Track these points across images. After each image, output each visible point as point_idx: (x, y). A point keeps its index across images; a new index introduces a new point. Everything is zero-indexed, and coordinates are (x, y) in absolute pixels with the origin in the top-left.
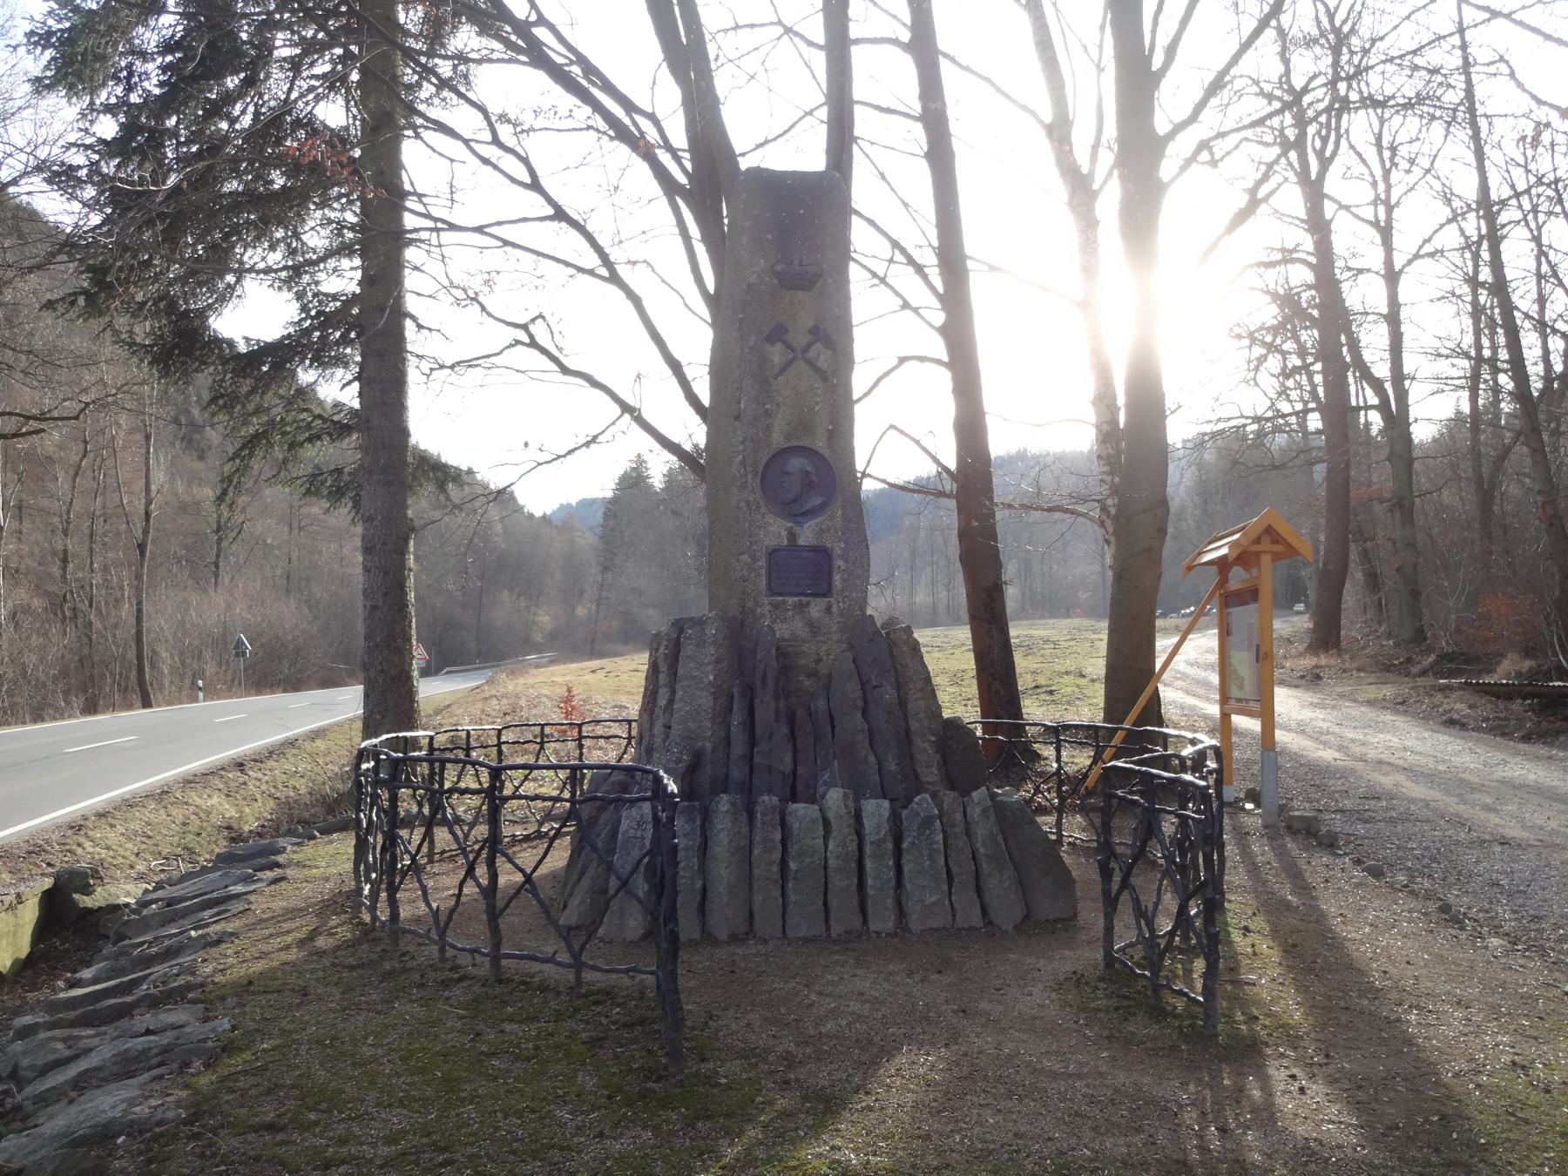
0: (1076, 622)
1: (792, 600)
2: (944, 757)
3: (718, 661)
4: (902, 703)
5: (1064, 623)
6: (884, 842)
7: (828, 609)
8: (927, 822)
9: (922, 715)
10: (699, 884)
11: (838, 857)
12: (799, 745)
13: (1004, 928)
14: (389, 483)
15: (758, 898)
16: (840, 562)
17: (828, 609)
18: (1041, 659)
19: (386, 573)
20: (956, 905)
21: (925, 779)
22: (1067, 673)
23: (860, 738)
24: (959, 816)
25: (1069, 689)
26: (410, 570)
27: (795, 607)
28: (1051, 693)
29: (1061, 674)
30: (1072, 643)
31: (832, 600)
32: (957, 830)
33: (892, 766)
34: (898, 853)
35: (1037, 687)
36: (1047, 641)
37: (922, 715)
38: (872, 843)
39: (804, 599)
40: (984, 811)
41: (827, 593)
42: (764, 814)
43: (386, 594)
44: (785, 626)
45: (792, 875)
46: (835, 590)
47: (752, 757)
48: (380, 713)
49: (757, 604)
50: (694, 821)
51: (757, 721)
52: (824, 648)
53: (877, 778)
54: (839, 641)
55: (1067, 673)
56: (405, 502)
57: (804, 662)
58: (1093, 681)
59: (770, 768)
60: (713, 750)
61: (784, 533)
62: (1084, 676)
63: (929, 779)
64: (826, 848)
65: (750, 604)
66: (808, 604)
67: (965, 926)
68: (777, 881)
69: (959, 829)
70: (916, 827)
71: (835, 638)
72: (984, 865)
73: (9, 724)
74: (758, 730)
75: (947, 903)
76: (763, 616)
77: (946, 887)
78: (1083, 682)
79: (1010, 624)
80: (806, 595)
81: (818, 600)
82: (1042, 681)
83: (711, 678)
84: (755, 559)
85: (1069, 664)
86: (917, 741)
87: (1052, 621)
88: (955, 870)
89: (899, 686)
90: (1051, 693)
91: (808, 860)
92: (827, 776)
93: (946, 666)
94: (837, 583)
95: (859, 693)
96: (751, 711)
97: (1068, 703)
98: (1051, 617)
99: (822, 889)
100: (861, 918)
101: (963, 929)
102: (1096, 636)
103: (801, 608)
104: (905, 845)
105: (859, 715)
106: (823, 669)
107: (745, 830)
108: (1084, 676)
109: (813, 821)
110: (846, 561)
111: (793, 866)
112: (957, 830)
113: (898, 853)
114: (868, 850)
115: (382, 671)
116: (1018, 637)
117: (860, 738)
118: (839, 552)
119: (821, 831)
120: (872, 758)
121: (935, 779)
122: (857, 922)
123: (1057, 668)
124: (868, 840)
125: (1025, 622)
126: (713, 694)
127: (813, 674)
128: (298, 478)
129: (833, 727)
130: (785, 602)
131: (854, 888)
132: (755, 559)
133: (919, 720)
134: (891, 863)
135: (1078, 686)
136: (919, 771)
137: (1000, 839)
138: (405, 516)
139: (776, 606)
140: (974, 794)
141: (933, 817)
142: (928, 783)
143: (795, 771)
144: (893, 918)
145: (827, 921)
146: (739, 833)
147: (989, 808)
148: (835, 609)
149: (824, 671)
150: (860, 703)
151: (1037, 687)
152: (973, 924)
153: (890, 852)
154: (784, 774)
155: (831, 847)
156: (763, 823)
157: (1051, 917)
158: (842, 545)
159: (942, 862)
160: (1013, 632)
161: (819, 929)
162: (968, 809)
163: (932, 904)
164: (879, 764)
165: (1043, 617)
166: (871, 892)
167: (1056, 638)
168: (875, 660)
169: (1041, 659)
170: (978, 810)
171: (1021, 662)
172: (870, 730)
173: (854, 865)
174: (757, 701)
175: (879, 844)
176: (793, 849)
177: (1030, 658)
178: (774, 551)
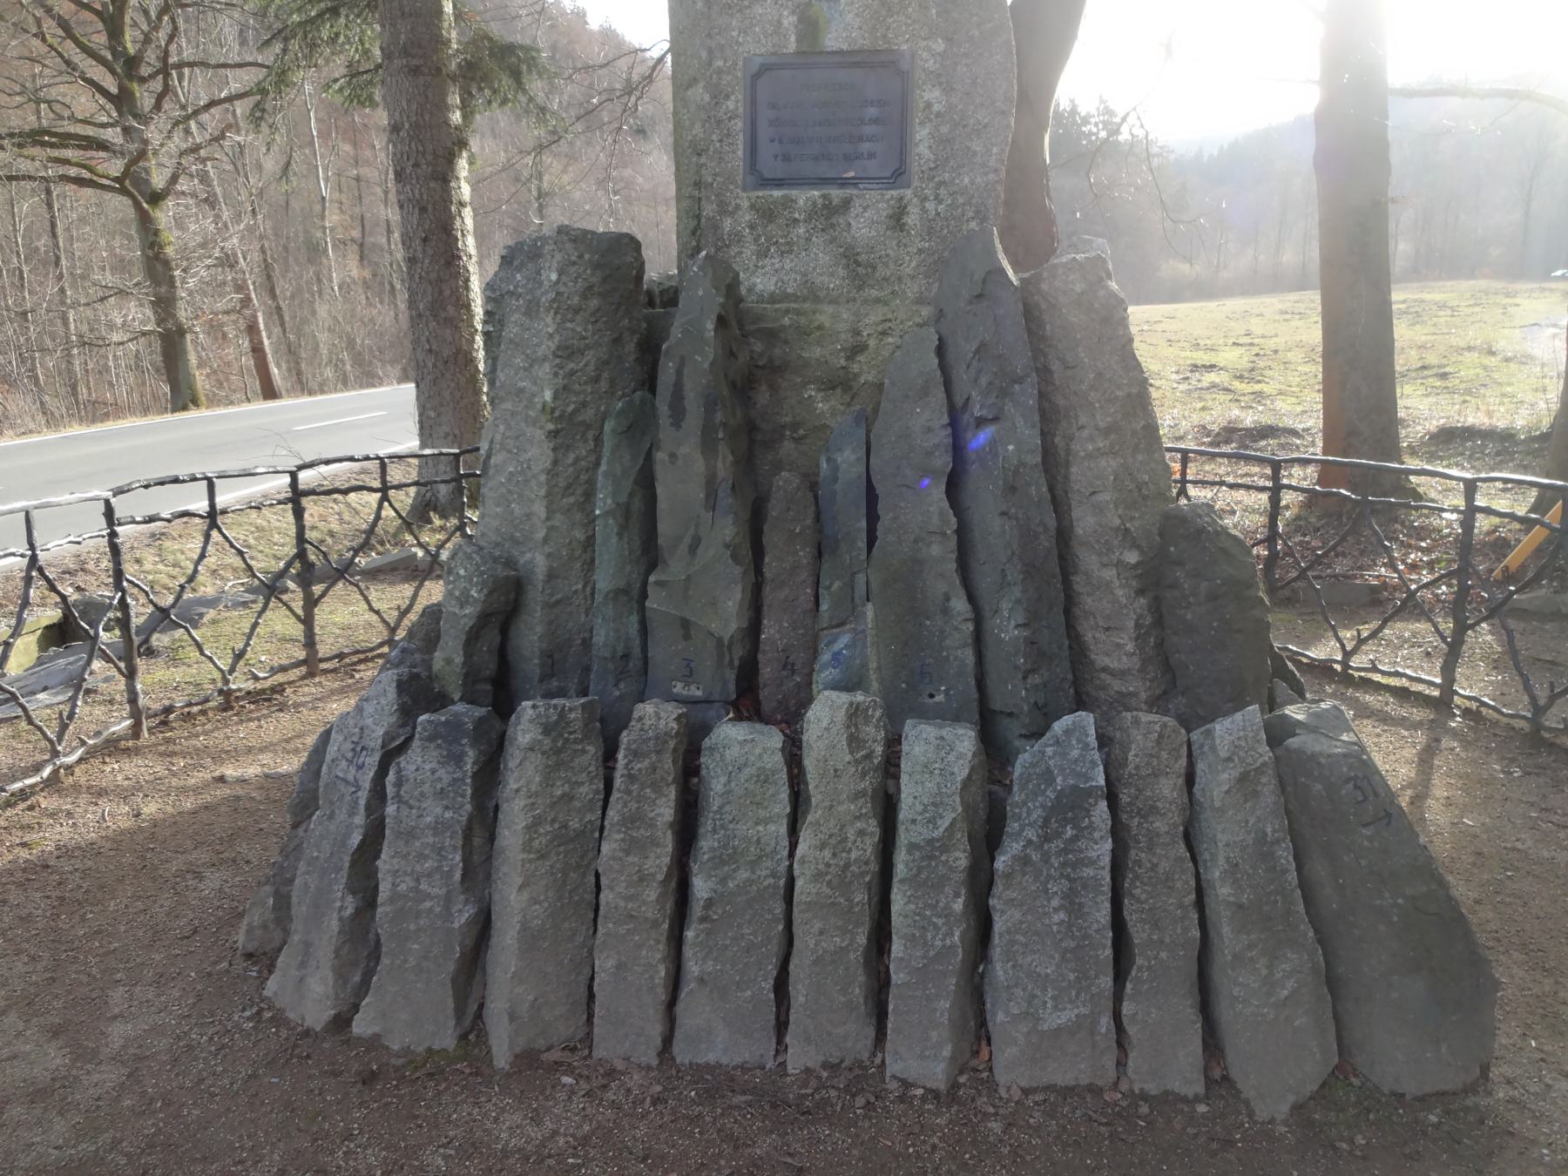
0: (1482, 283)
1: (805, 197)
2: (1158, 613)
3: (566, 352)
4: (1053, 462)
5: (1465, 285)
6: (945, 849)
7: (897, 219)
8: (1070, 806)
9: (1106, 497)
10: (464, 914)
11: (818, 877)
12: (771, 566)
13: (1262, 1114)
14: (415, 71)
15: (605, 964)
16: (931, 95)
17: (897, 219)
18: (1433, 330)
19: (423, 210)
20: (1131, 1030)
21: (1102, 660)
22: (1469, 349)
23: (935, 550)
24: (1168, 789)
25: (1472, 372)
26: (462, 204)
27: (813, 213)
28: (1444, 376)
29: (1460, 351)
30: (1477, 309)
31: (909, 193)
32: (1159, 825)
33: (1007, 627)
34: (981, 883)
35: (1424, 368)
36: (1442, 306)
37: (1106, 497)
38: (912, 847)
39: (836, 194)
40: (1243, 778)
41: (898, 176)
42: (636, 754)
43: (425, 240)
44: (788, 265)
45: (697, 910)
46: (914, 168)
47: (644, 595)
48: (433, 408)
49: (723, 209)
50: (458, 759)
51: (662, 505)
52: (875, 315)
53: (969, 656)
54: (920, 301)
55: (1469, 349)
56: (444, 100)
57: (817, 352)
58: (1507, 360)
59: (685, 624)
60: (551, 576)
61: (789, 20)
62: (1491, 353)
63: (1113, 664)
64: (793, 846)
65: (709, 209)
66: (846, 203)
67: (1152, 1088)
68: (655, 924)
69: (1166, 824)
70: (1037, 814)
71: (912, 289)
72: (1226, 930)
73: (232, 403)
74: (665, 527)
75: (1105, 1023)
76: (738, 238)
77: (1106, 982)
78: (1491, 361)
79: (1392, 286)
80: (844, 183)
81: (872, 196)
82: (1432, 359)
83: (548, 395)
84: (719, 95)
85: (1473, 335)
86: (1088, 560)
87: (1449, 283)
88: (1139, 933)
89: (1049, 417)
90: (1444, 376)
91: (744, 874)
92: (844, 640)
93: (1304, 338)
94: (923, 149)
95: (943, 436)
96: (646, 481)
97: (1468, 392)
98: (1450, 278)
99: (774, 948)
100: (871, 1032)
101: (1144, 1096)
102: (1508, 300)
103: (829, 213)
104: (1001, 862)
105: (938, 492)
106: (865, 370)
107: (589, 790)
108: (1491, 353)
109: (764, 778)
110: (949, 89)
111: (701, 887)
112: (1159, 825)
113: (981, 883)
114: (902, 862)
115: (430, 351)
116: (1404, 302)
117: (935, 550)
118: (930, 64)
119: (782, 806)
120: (960, 605)
121: (1124, 663)
122: (855, 1037)
123: (1454, 341)
124: (903, 837)
125: (1415, 285)
126: (553, 434)
127: (839, 383)
128: (336, 80)
129: (873, 518)
130: (788, 203)
131: (856, 956)
132: (719, 95)
133: (1099, 510)
134: (958, 905)
135: (1485, 368)
136: (1088, 637)
137: (1285, 855)
138: (447, 123)
139: (767, 214)
140: (1221, 727)
141: (1090, 792)
142: (1105, 669)
143: (753, 630)
144: (947, 1052)
145: (781, 1026)
146: (567, 798)
147: (1260, 771)
148: (912, 218)
149: (868, 377)
150: (944, 461)
151: (1424, 368)
152: (1177, 1086)
153: (960, 877)
154: (720, 641)
155: (801, 850)
156: (631, 778)
157: (1410, 1088)
158: (939, 45)
159: (1103, 914)
160: (1396, 296)
161: (755, 1049)
162: (1201, 767)
163: (1057, 1032)
164: (978, 620)
165: (1439, 278)
166: (897, 977)
167: (1455, 303)
168: (981, 348)
169: (1433, 330)
170: (1227, 776)
171: (1402, 332)
172: (963, 533)
173: (860, 896)
174: (660, 456)
175: (932, 850)
176: (707, 844)
177: (1418, 327)
178: (765, 69)
